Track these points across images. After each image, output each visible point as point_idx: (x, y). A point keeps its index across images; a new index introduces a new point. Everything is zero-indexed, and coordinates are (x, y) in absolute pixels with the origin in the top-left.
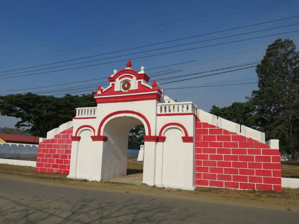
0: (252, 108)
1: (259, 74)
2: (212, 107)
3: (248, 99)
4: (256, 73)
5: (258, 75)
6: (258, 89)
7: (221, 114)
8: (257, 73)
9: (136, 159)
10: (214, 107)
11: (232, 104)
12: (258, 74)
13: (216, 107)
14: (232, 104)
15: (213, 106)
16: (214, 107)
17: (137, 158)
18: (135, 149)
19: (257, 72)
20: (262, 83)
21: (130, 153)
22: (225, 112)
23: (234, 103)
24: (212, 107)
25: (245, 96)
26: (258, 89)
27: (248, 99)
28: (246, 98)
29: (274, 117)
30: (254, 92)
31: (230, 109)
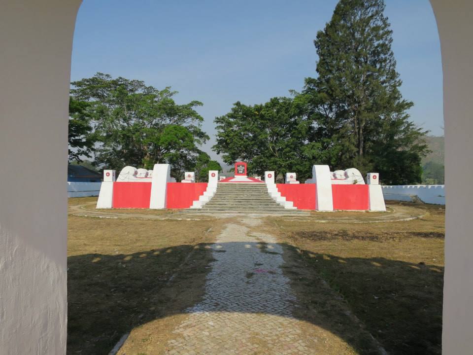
0: (255, 114)
1: (319, 49)
2: (234, 104)
3: (293, 93)
4: (314, 47)
5: (317, 51)
6: (316, 76)
7: (255, 115)
8: (316, 48)
9: (94, 203)
10: (238, 104)
11: (271, 99)
12: (317, 49)
13: (241, 104)
14: (271, 99)
15: (236, 102)
16: (238, 104)
17: (97, 200)
18: (87, 181)
19: (315, 45)
20: (322, 66)
21: (75, 190)
22: (261, 112)
23: (275, 98)
24: (234, 104)
25: (289, 89)
26: (316, 76)
27: (293, 93)
28: (291, 91)
29: (128, 89)
30: (310, 81)
31: (270, 107)
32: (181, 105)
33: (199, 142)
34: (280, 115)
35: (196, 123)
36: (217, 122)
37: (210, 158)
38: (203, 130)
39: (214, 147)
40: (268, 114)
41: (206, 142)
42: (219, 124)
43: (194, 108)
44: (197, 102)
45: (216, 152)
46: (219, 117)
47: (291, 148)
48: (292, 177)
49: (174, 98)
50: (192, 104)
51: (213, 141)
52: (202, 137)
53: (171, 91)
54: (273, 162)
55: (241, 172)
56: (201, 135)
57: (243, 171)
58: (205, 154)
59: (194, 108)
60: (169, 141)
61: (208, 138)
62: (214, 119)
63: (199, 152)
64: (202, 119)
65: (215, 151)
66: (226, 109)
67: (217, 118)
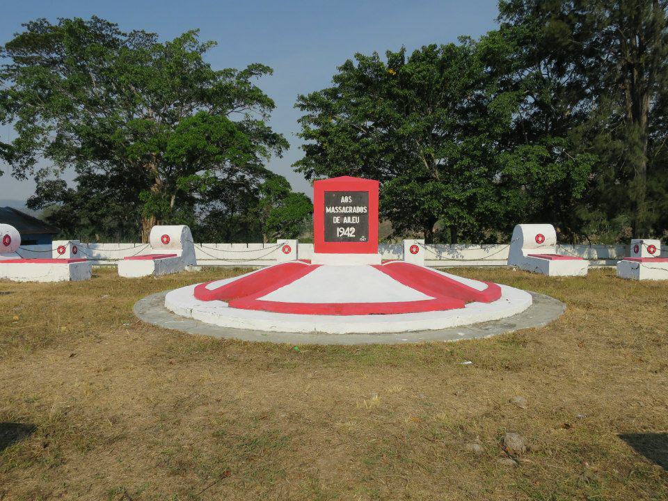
2: (340, 69)
24: (340, 69)
32: (222, 69)
33: (264, 152)
34: (446, 73)
35: (255, 113)
36: (303, 107)
37: (289, 187)
38: (276, 130)
39: (297, 164)
40: (419, 72)
41: (282, 154)
42: (306, 113)
43: (254, 81)
44: (260, 65)
45: (302, 175)
46: (306, 96)
47: (473, 157)
48: (540, 239)
49: (206, 58)
50: (249, 72)
51: (296, 153)
52: (274, 144)
53: (202, 39)
54: (431, 193)
55: (350, 232)
56: (274, 140)
57: (361, 229)
58: (281, 180)
59: (254, 81)
60: (188, 146)
61: (287, 146)
62: (294, 100)
63: (269, 175)
64: (271, 105)
65: (300, 171)
66: (323, 80)
67: (302, 98)
